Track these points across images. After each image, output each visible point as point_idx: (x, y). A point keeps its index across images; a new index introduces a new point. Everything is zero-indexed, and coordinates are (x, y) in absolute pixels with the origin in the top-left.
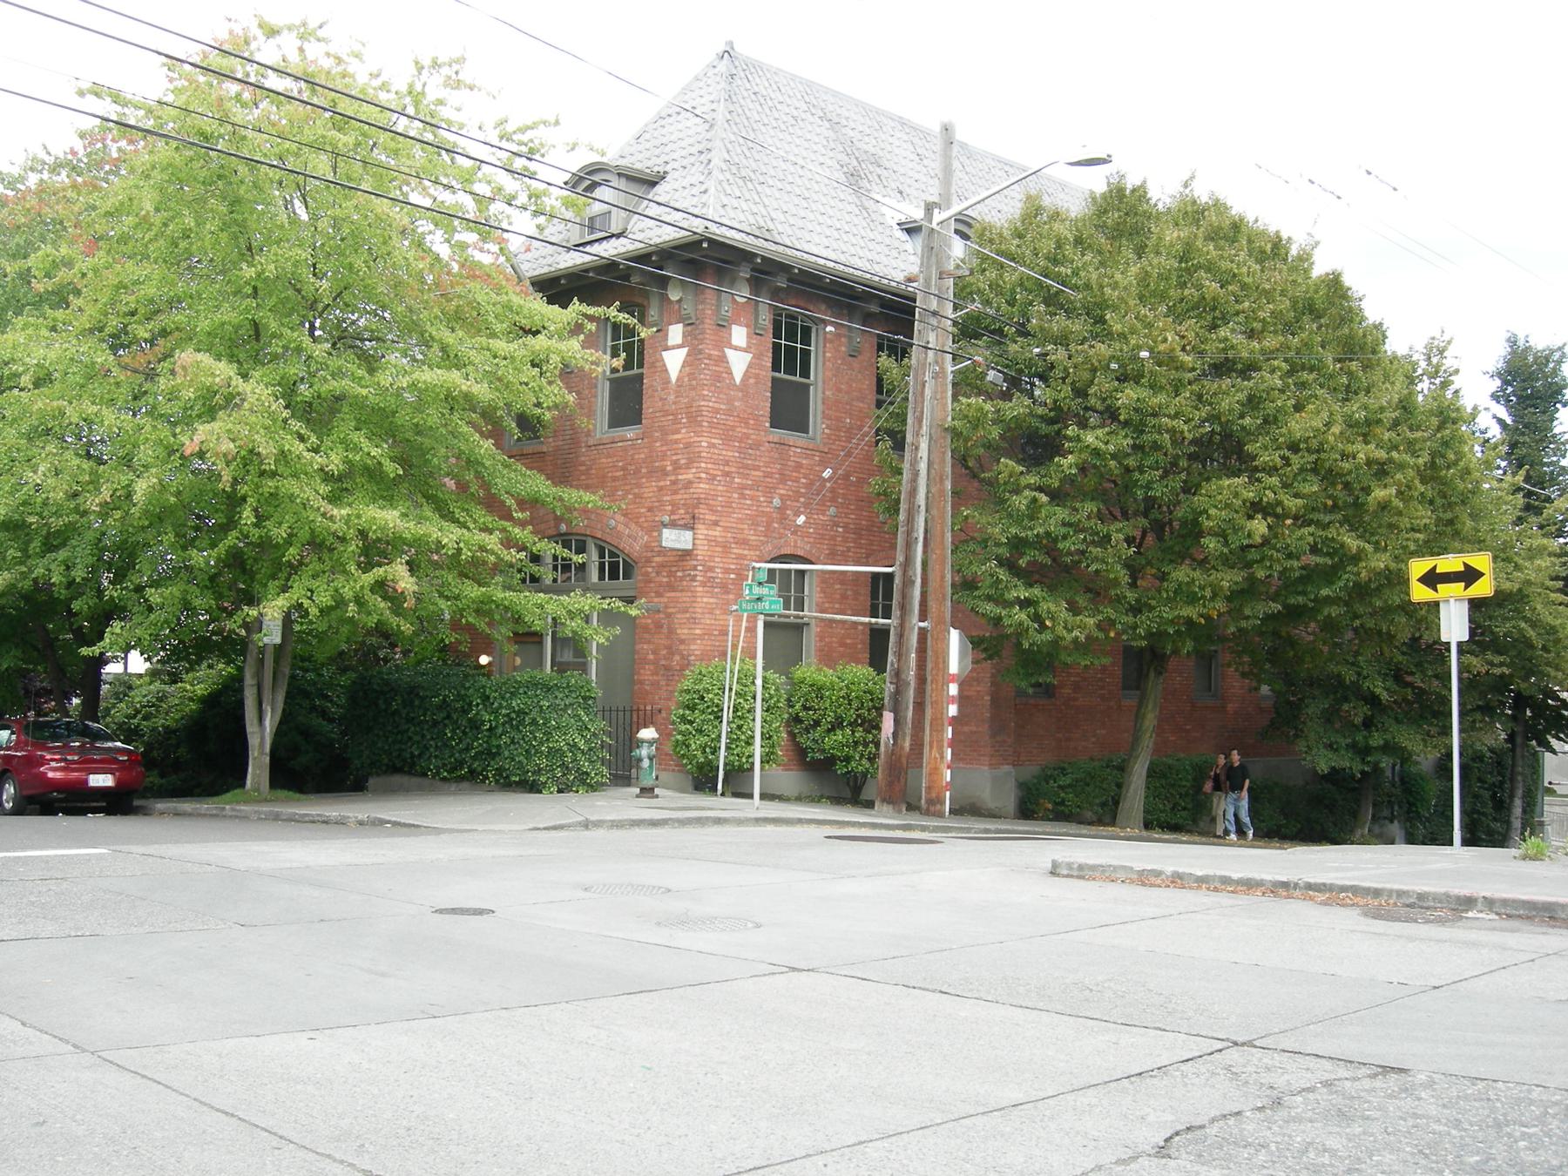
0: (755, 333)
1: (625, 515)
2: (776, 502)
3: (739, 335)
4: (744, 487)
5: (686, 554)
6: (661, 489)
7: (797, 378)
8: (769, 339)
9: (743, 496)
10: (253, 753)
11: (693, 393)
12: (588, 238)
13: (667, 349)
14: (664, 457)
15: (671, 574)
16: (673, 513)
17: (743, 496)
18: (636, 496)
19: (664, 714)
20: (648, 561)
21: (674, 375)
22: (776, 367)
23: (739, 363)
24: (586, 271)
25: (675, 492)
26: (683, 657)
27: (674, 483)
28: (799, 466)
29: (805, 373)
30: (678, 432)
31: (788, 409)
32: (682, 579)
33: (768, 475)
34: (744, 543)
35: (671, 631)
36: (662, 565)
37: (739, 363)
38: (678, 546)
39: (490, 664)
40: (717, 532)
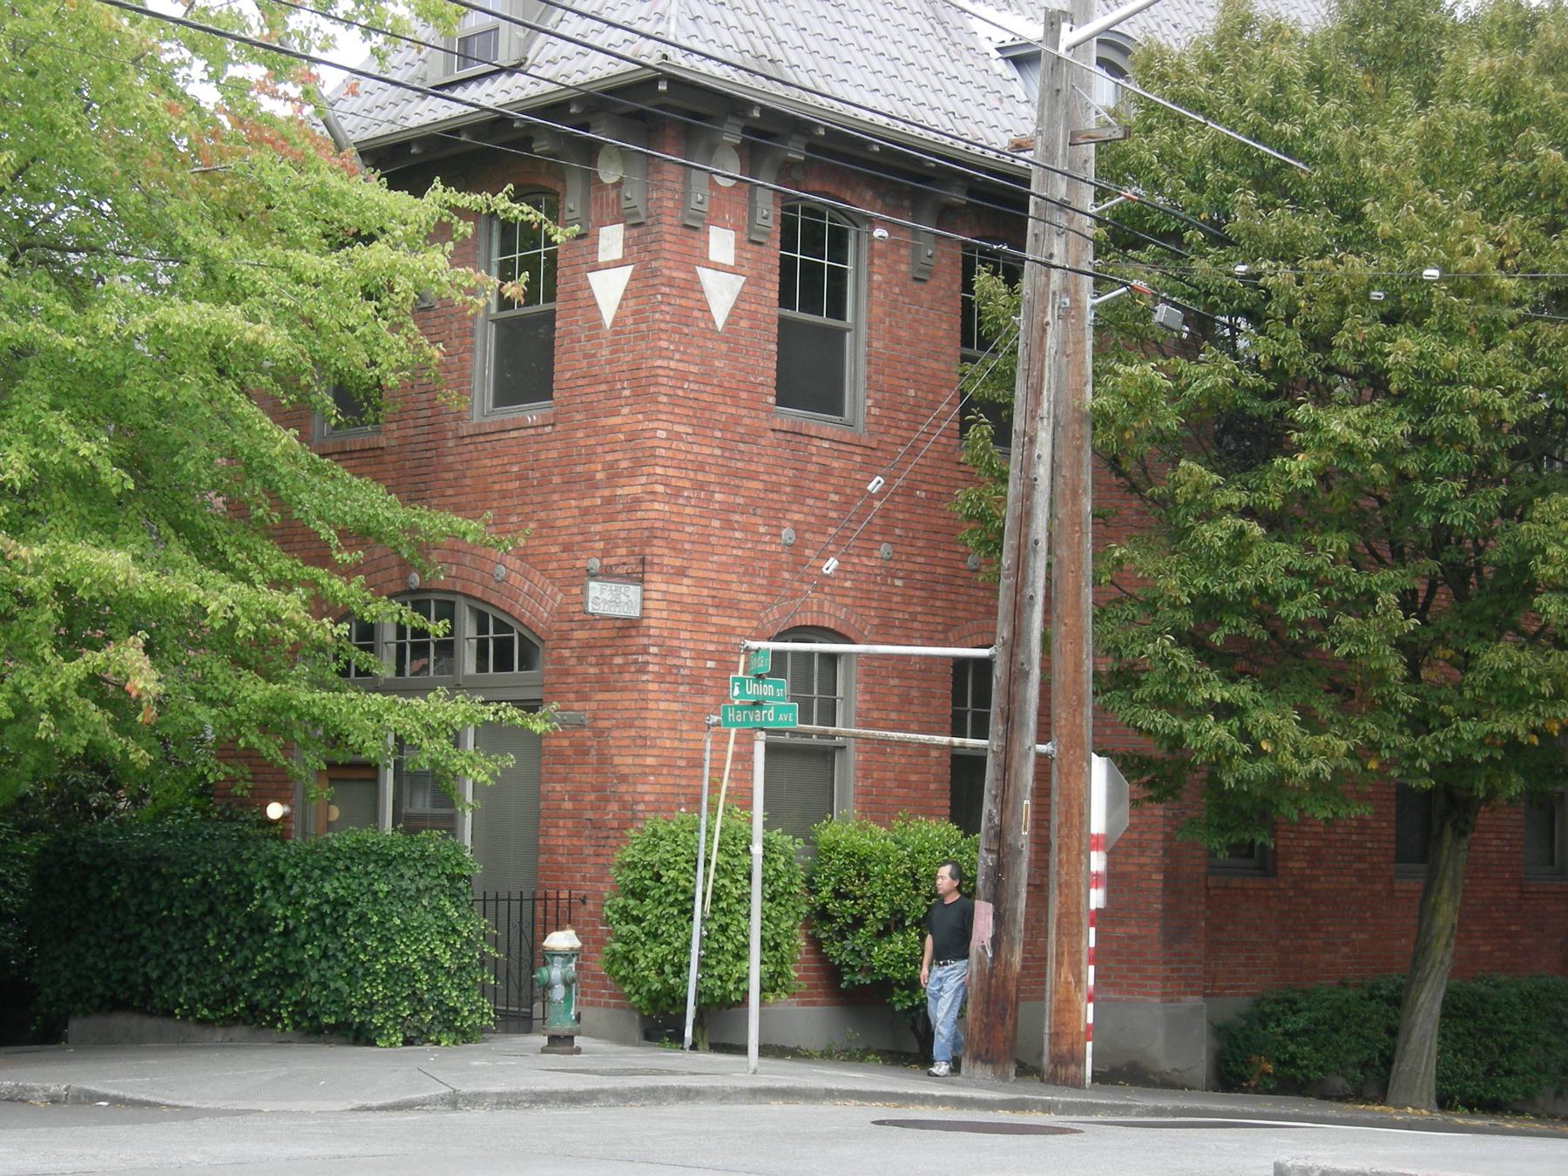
0: (750, 240)
1: (523, 557)
2: (787, 534)
3: (722, 244)
4: (730, 509)
5: (628, 627)
6: (585, 512)
7: (824, 320)
8: (774, 251)
9: (728, 525)
12: (459, 75)
13: (596, 268)
15: (603, 661)
16: (606, 553)
18: (543, 524)
19: (590, 906)
21: (608, 312)
22: (785, 300)
23: (721, 292)
25: (610, 518)
26: (624, 806)
27: (609, 501)
28: (826, 471)
29: (838, 311)
31: (808, 374)
32: (622, 669)
35: (604, 760)
36: (588, 646)
37: (721, 292)
39: (285, 818)
40: (684, 588)
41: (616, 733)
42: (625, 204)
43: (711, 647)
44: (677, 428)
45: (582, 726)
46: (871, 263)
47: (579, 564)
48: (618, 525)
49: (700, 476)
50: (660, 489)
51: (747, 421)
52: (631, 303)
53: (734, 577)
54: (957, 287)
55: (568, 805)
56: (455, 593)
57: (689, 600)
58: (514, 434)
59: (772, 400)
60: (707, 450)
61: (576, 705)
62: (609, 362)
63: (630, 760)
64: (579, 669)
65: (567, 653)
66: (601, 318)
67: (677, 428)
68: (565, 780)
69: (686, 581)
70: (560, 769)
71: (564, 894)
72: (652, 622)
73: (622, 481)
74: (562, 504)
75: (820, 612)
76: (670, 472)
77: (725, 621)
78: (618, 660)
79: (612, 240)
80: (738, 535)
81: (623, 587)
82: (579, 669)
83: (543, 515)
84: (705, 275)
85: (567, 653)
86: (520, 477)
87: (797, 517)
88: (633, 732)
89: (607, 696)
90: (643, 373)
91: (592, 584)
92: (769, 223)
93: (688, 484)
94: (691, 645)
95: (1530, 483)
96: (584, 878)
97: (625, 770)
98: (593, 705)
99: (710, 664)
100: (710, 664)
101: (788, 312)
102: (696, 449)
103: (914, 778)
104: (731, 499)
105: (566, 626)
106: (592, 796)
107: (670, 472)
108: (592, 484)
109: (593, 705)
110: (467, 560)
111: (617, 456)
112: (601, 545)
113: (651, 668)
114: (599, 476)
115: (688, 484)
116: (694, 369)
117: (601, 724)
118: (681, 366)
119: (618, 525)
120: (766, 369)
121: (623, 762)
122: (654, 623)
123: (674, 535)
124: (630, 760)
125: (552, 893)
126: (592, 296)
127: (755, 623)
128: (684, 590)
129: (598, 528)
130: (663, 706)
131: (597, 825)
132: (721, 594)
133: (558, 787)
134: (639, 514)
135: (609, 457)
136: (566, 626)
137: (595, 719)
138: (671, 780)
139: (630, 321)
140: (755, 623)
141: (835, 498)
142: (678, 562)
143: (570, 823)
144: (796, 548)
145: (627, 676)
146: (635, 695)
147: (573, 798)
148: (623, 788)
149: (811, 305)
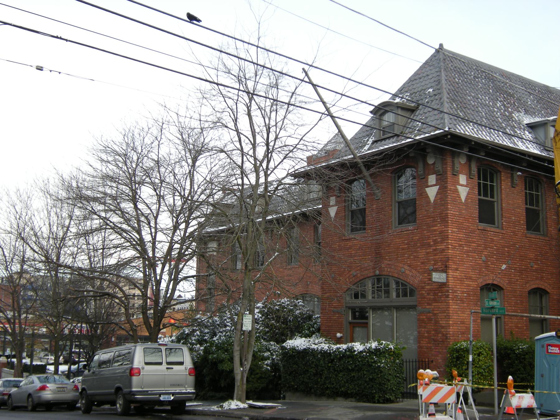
0: (470, 177)
1: (409, 266)
2: (484, 258)
3: (463, 179)
4: (468, 251)
5: (442, 285)
6: (428, 253)
7: (489, 199)
8: (476, 180)
9: (468, 256)
10: (238, 383)
11: (443, 207)
12: (383, 137)
13: (428, 187)
14: (429, 238)
15: (435, 294)
16: (434, 264)
17: (468, 256)
18: (415, 257)
19: (434, 363)
20: (423, 288)
21: (432, 199)
22: (479, 194)
23: (463, 192)
24: (403, 147)
25: (436, 255)
26: (443, 335)
27: (435, 250)
28: (492, 240)
29: (492, 196)
30: (435, 226)
31: (487, 213)
32: (441, 297)
33: (479, 245)
34: (470, 278)
35: (437, 322)
36: (430, 290)
37: (463, 192)
38: (440, 281)
39: (341, 337)
40: (457, 274)
41: (440, 315)
42: (436, 169)
43: (465, 290)
44: (454, 230)
45: (429, 312)
46: (501, 183)
47: (427, 267)
48: (438, 257)
49: (460, 243)
50: (450, 246)
51: (471, 227)
52: (439, 196)
53: (470, 270)
54: (523, 189)
55: (426, 335)
56: (390, 276)
57: (459, 277)
58: (405, 232)
59: (478, 221)
60: (462, 236)
61: (427, 307)
62: (433, 212)
63: (444, 322)
64: (428, 297)
65: (424, 292)
66: (430, 200)
67: (454, 230)
68: (425, 328)
69: (458, 272)
70: (423, 324)
71: (427, 360)
72: (450, 284)
73: (439, 245)
74: (420, 251)
75: (493, 280)
76: (453, 242)
77: (469, 283)
78: (440, 294)
79: (432, 179)
80: (471, 259)
81: (441, 274)
82: (428, 297)
83: (415, 254)
84: (459, 188)
85: (424, 292)
86: (407, 244)
87: (486, 253)
88: (445, 314)
89: (437, 304)
90: (443, 215)
91: (433, 273)
92: (475, 173)
93: (457, 245)
94: (460, 290)
95: (65, 255)
96: (432, 355)
97: (444, 325)
98: (433, 307)
99: (465, 295)
100: (465, 295)
101: (480, 197)
102: (459, 235)
103: (519, 325)
104: (468, 249)
105: (423, 285)
106: (433, 332)
107: (453, 242)
108: (430, 246)
109: (433, 307)
110: (393, 267)
111: (437, 238)
112: (433, 262)
113: (450, 296)
114: (432, 243)
115: (457, 245)
116: (457, 213)
117: (435, 312)
118: (454, 213)
119: (438, 257)
120: (476, 213)
121: (443, 323)
122: (451, 284)
123: (454, 259)
124: (444, 322)
125: (424, 360)
126: (427, 194)
127: (476, 283)
128: (457, 274)
129: (432, 258)
130: (454, 307)
131: (435, 340)
132: (467, 275)
133: (423, 330)
134: (444, 254)
135: (434, 238)
136: (423, 285)
137: (433, 310)
138: (456, 328)
139: (439, 201)
140: (476, 283)
141: (495, 248)
142: (456, 267)
143: (427, 340)
144: (485, 262)
145: (443, 299)
146: (445, 304)
147: (428, 332)
148: (443, 330)
149: (486, 195)
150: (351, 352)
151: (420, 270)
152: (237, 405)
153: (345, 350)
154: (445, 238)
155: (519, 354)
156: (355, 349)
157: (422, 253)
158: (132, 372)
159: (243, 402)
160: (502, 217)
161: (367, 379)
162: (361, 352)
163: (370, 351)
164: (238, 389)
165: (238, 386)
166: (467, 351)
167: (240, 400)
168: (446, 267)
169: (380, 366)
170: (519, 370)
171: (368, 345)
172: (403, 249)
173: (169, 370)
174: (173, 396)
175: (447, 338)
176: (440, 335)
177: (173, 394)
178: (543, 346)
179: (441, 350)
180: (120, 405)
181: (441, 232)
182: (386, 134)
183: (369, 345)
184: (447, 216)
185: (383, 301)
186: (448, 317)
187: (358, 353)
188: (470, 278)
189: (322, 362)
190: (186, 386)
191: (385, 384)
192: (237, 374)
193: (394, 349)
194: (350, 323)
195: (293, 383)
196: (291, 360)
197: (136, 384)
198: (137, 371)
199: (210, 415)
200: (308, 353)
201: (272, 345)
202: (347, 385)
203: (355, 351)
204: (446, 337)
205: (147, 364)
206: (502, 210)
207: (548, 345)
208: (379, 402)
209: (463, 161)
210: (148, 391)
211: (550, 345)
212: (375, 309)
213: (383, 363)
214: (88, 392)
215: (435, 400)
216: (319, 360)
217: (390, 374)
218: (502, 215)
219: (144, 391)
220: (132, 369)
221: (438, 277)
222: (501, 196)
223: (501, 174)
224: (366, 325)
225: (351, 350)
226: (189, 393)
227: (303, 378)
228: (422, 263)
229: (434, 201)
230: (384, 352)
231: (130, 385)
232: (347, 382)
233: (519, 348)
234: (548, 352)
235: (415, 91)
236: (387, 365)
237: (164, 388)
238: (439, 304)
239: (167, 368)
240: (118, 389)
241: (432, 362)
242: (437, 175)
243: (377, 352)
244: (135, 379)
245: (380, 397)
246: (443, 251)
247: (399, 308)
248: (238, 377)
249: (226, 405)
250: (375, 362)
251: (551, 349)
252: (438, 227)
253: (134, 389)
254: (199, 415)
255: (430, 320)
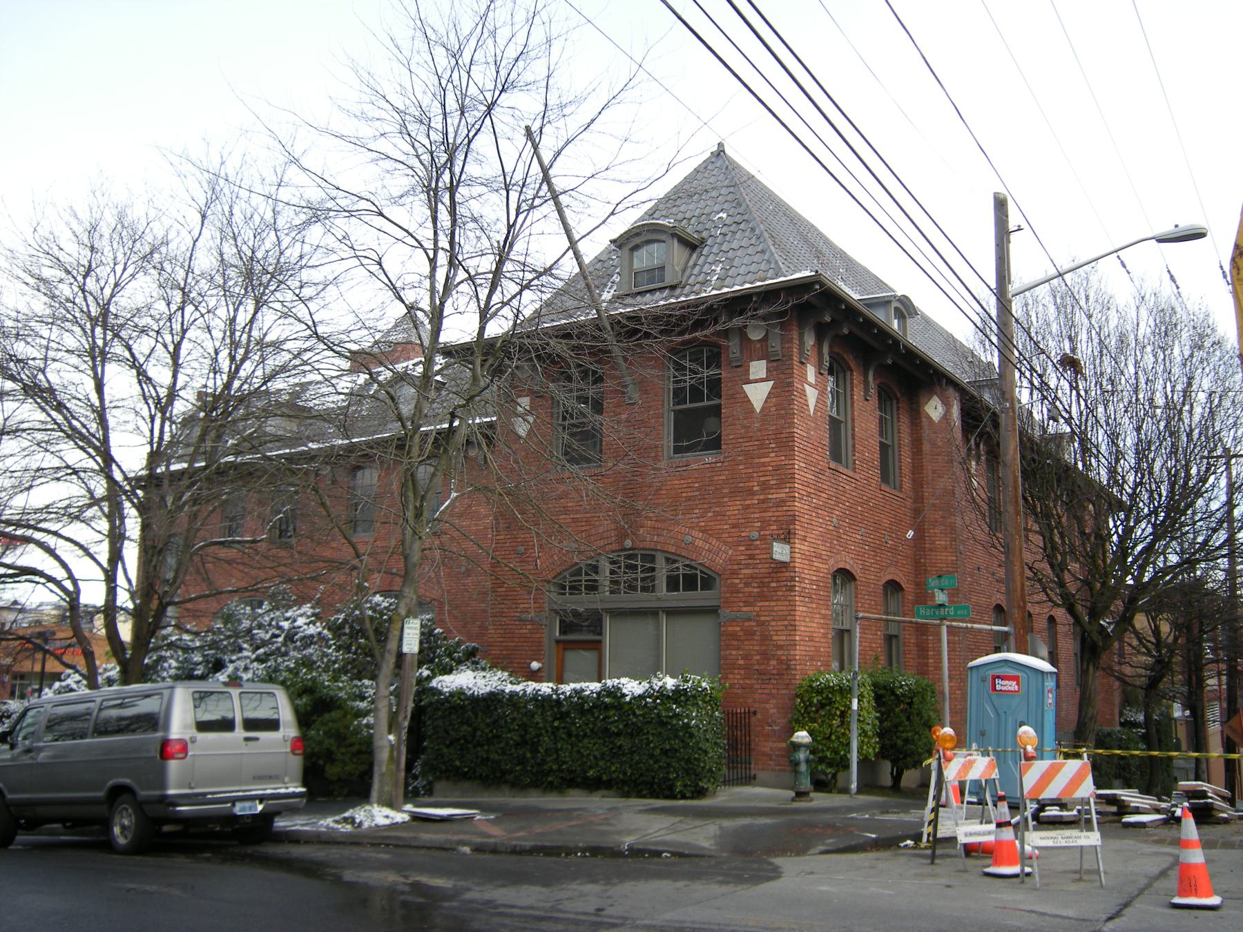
5: (783, 565)
6: (748, 507)
12: (635, 290)
14: (750, 478)
15: (762, 585)
16: (762, 528)
18: (716, 514)
19: (759, 716)
20: (735, 573)
21: (758, 405)
26: (780, 662)
27: (763, 501)
32: (776, 590)
34: (819, 556)
35: (765, 638)
37: (812, 395)
41: (773, 623)
45: (749, 620)
55: (742, 662)
61: (745, 609)
62: (760, 430)
65: (737, 581)
68: (738, 649)
78: (773, 585)
79: (758, 368)
85: (737, 581)
105: (736, 567)
108: (752, 493)
121: (780, 638)
136: (736, 567)
145: (780, 593)
147: (745, 657)
148: (779, 653)
150: (615, 697)
151: (730, 540)
152: (387, 817)
153: (599, 694)
154: (785, 477)
155: (903, 695)
156: (625, 691)
157: (733, 508)
158: (165, 750)
159: (400, 810)
160: (854, 451)
161: (657, 752)
162: (641, 697)
163: (662, 695)
164: (381, 781)
165: (383, 775)
166: (845, 692)
167: (390, 804)
168: (789, 533)
169: (688, 724)
170: (900, 724)
171: (657, 684)
172: (689, 499)
173: (250, 743)
174: (261, 803)
175: (789, 668)
176: (773, 662)
177: (261, 799)
178: (984, 680)
179: (775, 691)
180: (123, 828)
181: (777, 469)
182: (654, 279)
183: (660, 684)
184: (791, 436)
185: (639, 599)
186: (793, 627)
187: (634, 698)
188: (819, 556)
189: (538, 719)
190: (286, 779)
191: (698, 760)
192: (383, 747)
193: (712, 688)
194: (558, 642)
195: (458, 763)
196: (454, 717)
197: (177, 780)
198: (178, 747)
199: (343, 843)
200: (500, 701)
201: (367, 687)
202: (601, 763)
203: (624, 695)
204: (786, 666)
205: (203, 726)
206: (853, 439)
207: (994, 678)
208: (684, 797)
209: (810, 341)
210: (205, 794)
211: (998, 677)
212: (620, 614)
213: (694, 718)
214: (9, 796)
215: (1051, 792)
216: (531, 715)
217: (707, 740)
218: (854, 446)
219: (197, 795)
220: (165, 743)
221: (780, 551)
222: (853, 414)
223: (852, 375)
224: (596, 646)
225: (615, 693)
226: (294, 795)
227: (488, 751)
228: (734, 526)
229: (763, 409)
230: (694, 697)
231: (161, 780)
232: (603, 759)
233: (901, 686)
234: (994, 689)
235: (687, 216)
236: (701, 721)
237: (240, 784)
238: (773, 604)
239: (247, 739)
240: (118, 793)
241: (755, 713)
242: (769, 361)
243: (678, 695)
244: (173, 766)
245: (685, 786)
246: (782, 502)
247: (672, 612)
248: (383, 755)
249: (360, 814)
250: (676, 716)
251: (1001, 685)
252: (771, 458)
253: (171, 792)
254: (307, 842)
255: (750, 633)
